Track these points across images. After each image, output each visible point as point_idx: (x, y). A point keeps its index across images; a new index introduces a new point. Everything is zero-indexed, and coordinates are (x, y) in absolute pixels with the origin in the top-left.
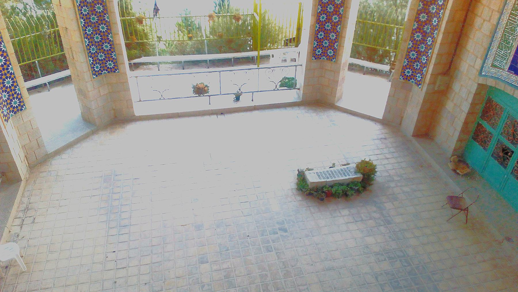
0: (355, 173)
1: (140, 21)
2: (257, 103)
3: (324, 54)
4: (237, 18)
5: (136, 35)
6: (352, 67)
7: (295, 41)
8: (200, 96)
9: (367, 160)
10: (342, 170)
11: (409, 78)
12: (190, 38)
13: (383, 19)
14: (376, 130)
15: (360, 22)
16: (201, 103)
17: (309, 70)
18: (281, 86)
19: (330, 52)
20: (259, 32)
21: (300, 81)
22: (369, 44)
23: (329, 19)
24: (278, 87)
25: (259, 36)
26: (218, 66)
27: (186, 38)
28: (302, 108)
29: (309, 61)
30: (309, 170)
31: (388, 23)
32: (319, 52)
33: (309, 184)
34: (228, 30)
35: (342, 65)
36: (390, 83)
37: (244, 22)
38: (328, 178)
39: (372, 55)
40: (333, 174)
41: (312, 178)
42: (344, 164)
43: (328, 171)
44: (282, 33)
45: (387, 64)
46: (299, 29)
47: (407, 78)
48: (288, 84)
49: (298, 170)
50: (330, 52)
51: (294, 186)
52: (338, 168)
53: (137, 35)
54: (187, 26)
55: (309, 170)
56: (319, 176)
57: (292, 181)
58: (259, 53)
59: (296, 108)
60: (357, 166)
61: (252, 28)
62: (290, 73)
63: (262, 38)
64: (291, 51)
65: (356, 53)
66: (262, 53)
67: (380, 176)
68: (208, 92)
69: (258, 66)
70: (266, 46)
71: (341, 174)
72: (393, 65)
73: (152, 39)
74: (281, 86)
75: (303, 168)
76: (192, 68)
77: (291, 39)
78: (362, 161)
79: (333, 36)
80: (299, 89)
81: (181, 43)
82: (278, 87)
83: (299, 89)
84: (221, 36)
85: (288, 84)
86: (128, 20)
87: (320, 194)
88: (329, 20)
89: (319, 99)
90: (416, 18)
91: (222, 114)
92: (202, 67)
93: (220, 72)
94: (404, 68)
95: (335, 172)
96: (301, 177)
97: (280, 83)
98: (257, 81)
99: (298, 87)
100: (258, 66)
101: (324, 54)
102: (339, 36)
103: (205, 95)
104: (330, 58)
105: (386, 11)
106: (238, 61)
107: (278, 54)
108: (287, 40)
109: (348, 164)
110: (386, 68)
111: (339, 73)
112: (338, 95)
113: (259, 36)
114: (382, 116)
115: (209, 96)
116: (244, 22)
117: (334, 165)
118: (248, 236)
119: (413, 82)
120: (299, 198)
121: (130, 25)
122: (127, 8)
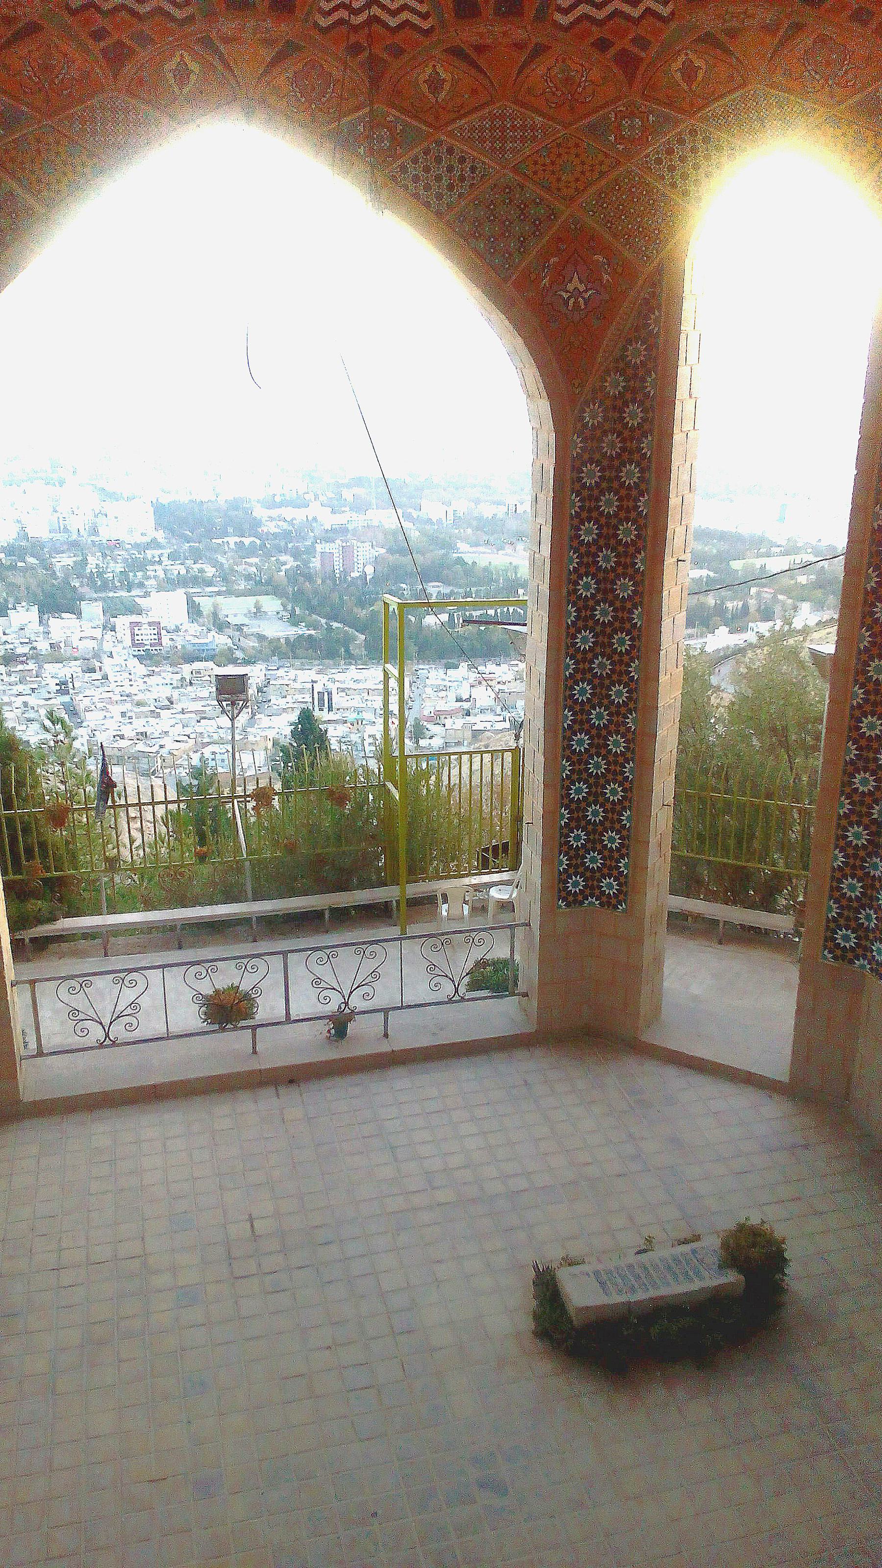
0: (720, 1267)
1: (59, 816)
2: (401, 1042)
3: (592, 888)
4: (339, 798)
5: (44, 855)
6: (680, 923)
7: (503, 854)
8: (223, 1030)
9: (755, 1220)
10: (676, 1260)
11: (850, 955)
12: (202, 858)
13: (755, 786)
14: (768, 1116)
15: (688, 797)
16: (230, 1049)
17: (550, 939)
18: (474, 986)
19: (609, 886)
20: (401, 830)
21: (529, 970)
22: (726, 852)
23: (596, 794)
24: (462, 990)
25: (402, 845)
26: (284, 934)
27: (189, 858)
28: (538, 1052)
29: (548, 911)
30: (570, 1262)
31: (769, 796)
32: (575, 884)
33: (572, 1312)
34: (313, 830)
35: (647, 920)
36: (793, 974)
37: (360, 806)
38: (633, 1290)
39: (737, 886)
40: (648, 1275)
41: (582, 1294)
42: (682, 1236)
43: (630, 1266)
44: (469, 834)
45: (785, 911)
46: (518, 819)
47: (843, 955)
48: (492, 979)
49: (536, 1267)
50: (609, 886)
51: (527, 1324)
52: (663, 1253)
53: (47, 857)
54: (199, 822)
55: (570, 1262)
56: (602, 1284)
57: (508, 1311)
58: (403, 891)
59: (520, 1053)
60: (725, 1246)
61: (381, 821)
62: (499, 950)
63: (410, 852)
64: (499, 887)
65: (687, 881)
66: (415, 890)
67: (800, 1279)
68: (249, 1015)
69: (403, 932)
70: (424, 870)
71: (675, 1276)
72: (800, 910)
73: (89, 863)
74: (474, 986)
75: (553, 1254)
76: (205, 945)
77: (495, 848)
78: (741, 1228)
79: (612, 840)
80: (525, 995)
81: (175, 873)
82: (462, 990)
83: (525, 995)
84: (291, 849)
85: (492, 979)
86: (21, 817)
87: (609, 1346)
88: (596, 796)
89: (588, 1018)
90: (843, 785)
91: (291, 1082)
92: (237, 939)
93: (284, 954)
94: (832, 926)
95: (656, 1267)
96: (547, 1289)
97: (467, 980)
98: (397, 980)
99: (522, 987)
100: (403, 932)
101: (592, 888)
102: (632, 841)
103: (243, 1023)
104: (609, 903)
105: (762, 765)
106: (342, 917)
107: (457, 891)
108: (486, 850)
109: (697, 1238)
110: (781, 922)
111: (640, 941)
112: (645, 1008)
113: (402, 845)
114: (787, 1069)
115: (254, 1028)
116: (360, 806)
117: (648, 1246)
118: (374, 1515)
119: (862, 967)
120: (545, 1366)
121: (26, 830)
122: (20, 784)
